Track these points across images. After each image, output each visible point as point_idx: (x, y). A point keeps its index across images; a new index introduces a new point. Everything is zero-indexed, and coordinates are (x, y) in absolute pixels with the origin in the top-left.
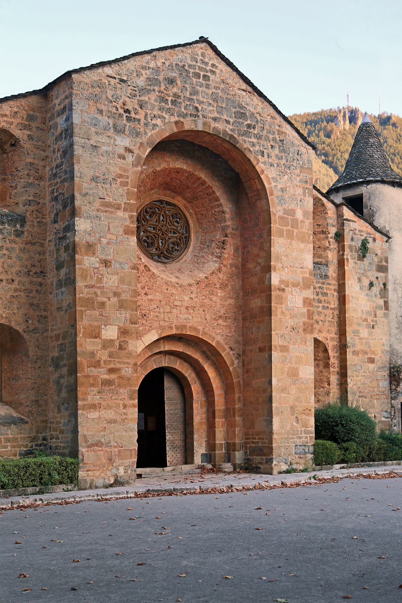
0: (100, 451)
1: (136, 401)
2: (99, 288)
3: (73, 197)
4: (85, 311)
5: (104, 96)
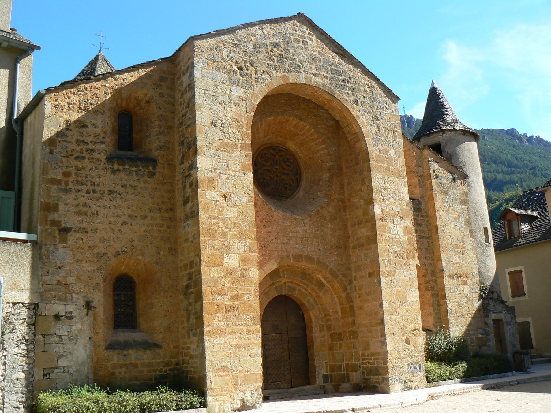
0: (226, 375)
1: (259, 327)
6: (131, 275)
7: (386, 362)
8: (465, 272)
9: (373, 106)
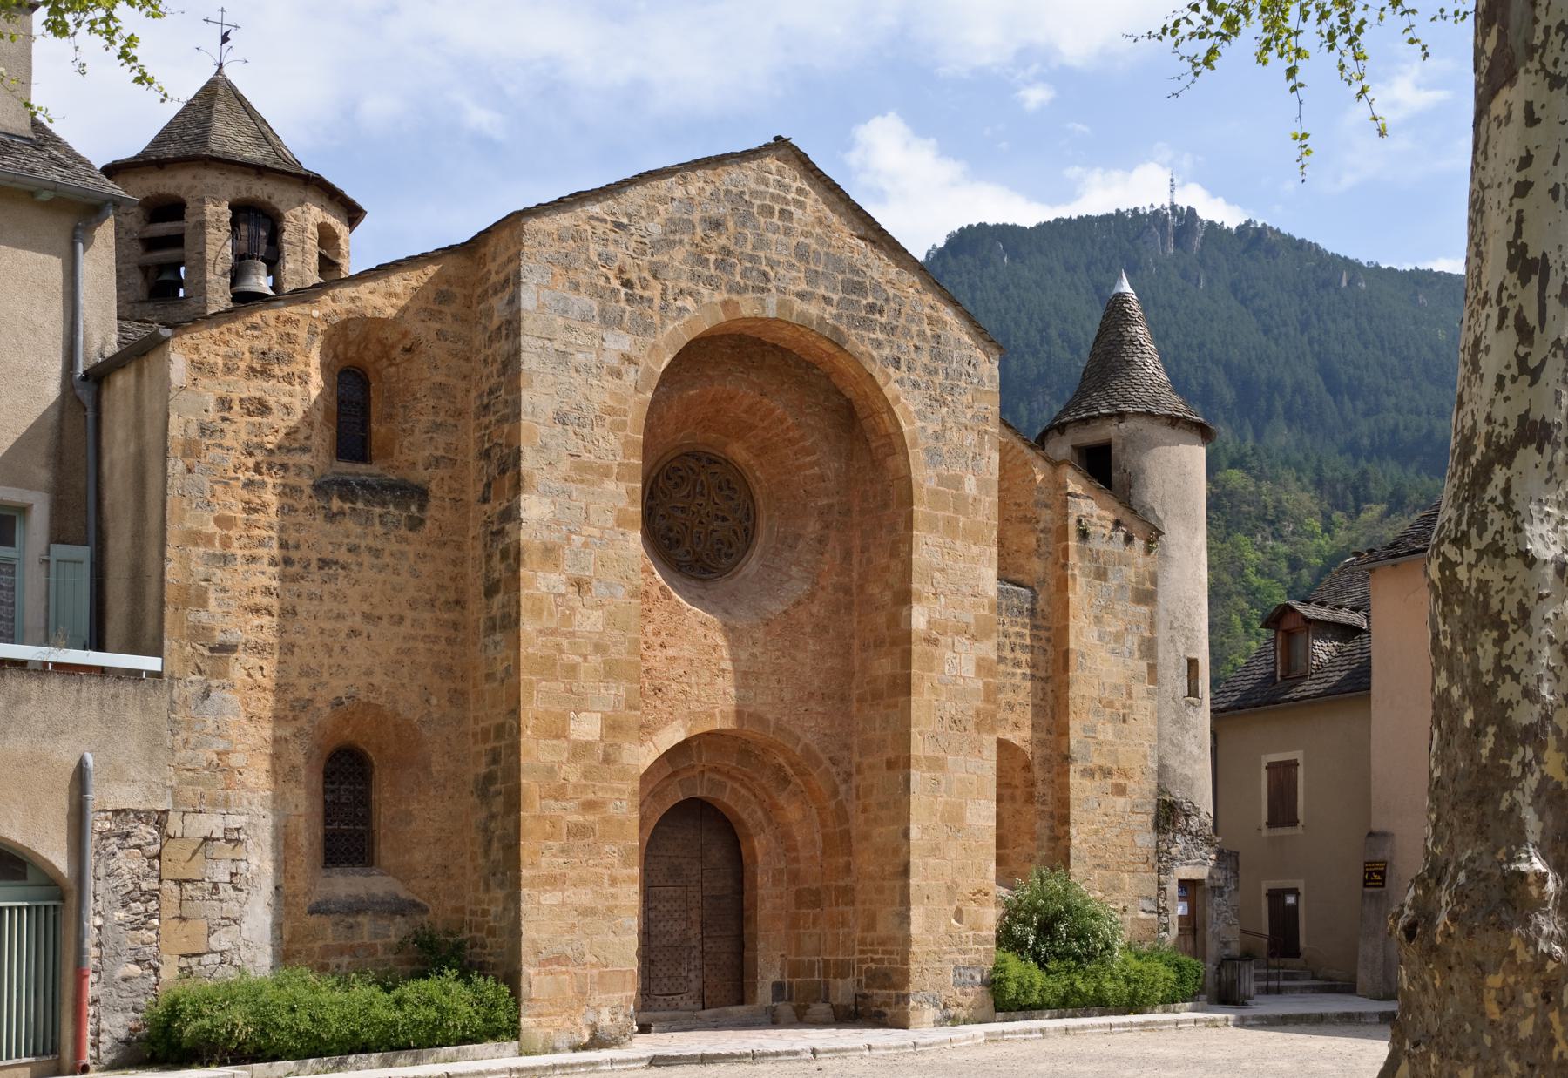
0: (563, 973)
1: (636, 871)
2: (564, 635)
3: (518, 454)
4: (538, 682)
5: (583, 256)
6: (362, 746)
7: (905, 961)
8: (1124, 765)
9: (936, 372)
